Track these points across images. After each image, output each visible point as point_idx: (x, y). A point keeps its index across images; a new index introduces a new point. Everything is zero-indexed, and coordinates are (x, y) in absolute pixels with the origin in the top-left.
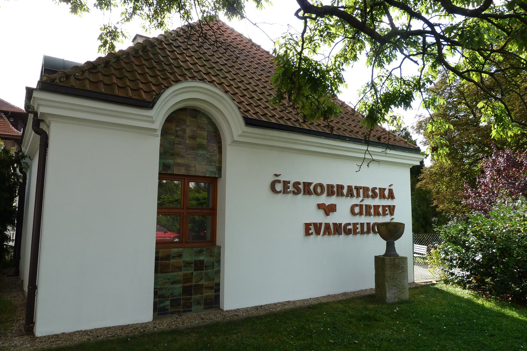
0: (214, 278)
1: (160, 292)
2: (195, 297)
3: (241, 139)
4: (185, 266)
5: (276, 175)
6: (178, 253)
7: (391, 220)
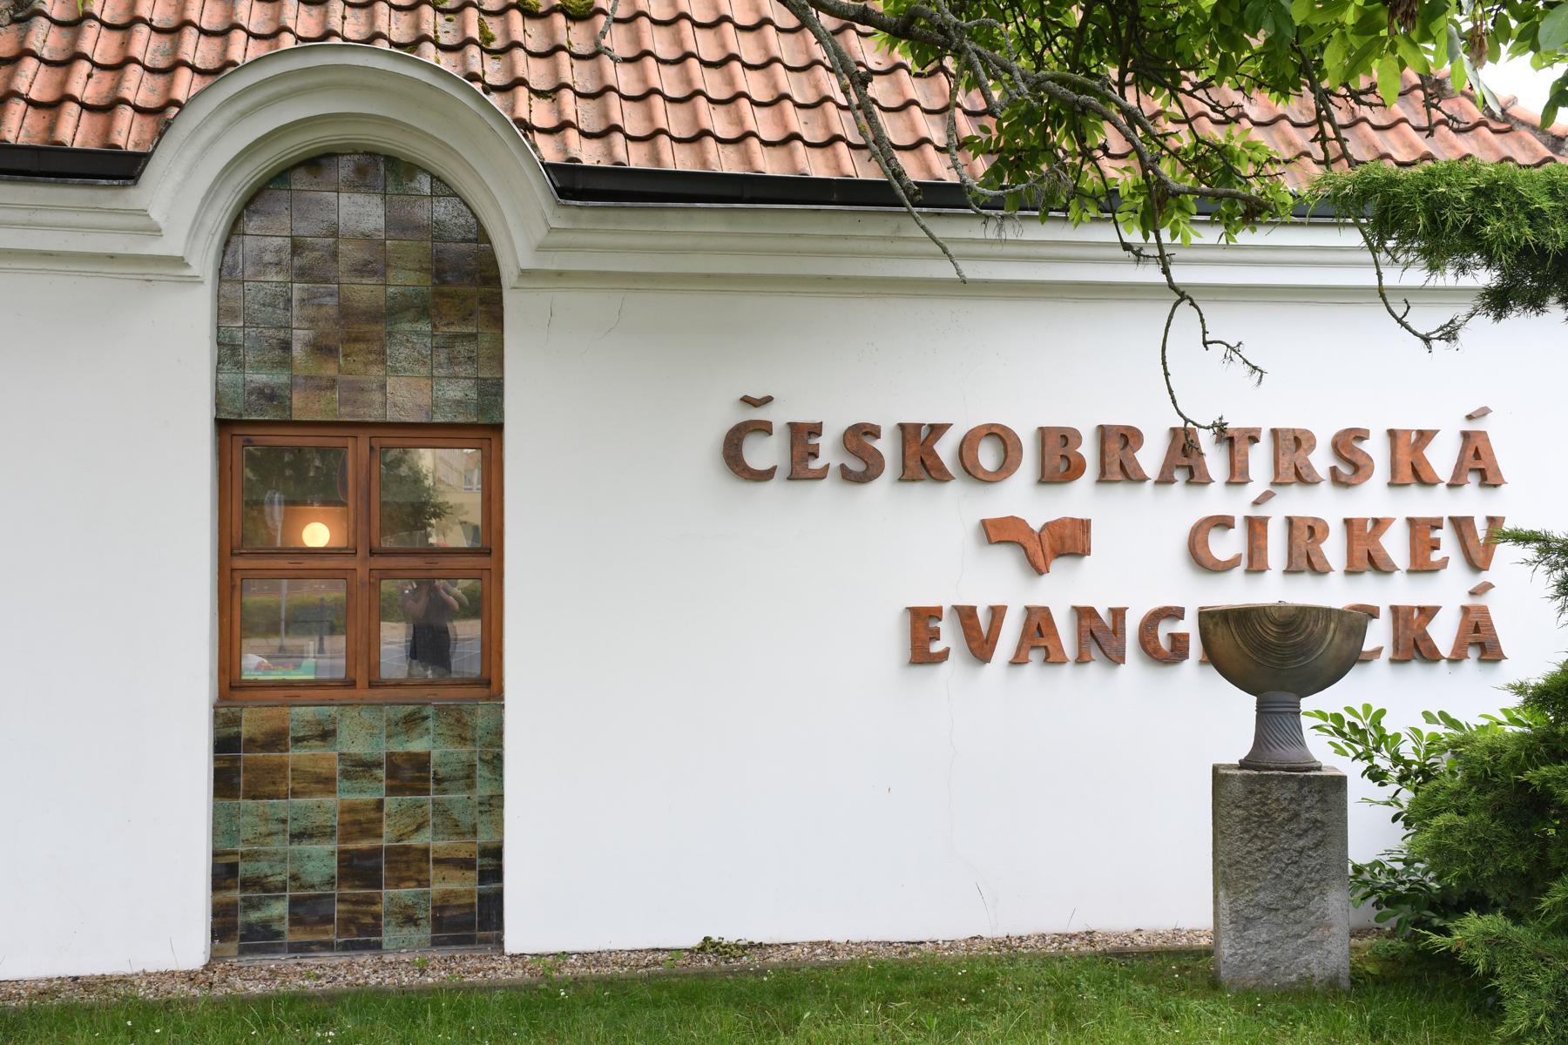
0: (475, 825)
1: (232, 869)
2: (392, 895)
3: (553, 263)
4: (346, 775)
5: (747, 401)
6: (319, 723)
7: (1473, 593)
